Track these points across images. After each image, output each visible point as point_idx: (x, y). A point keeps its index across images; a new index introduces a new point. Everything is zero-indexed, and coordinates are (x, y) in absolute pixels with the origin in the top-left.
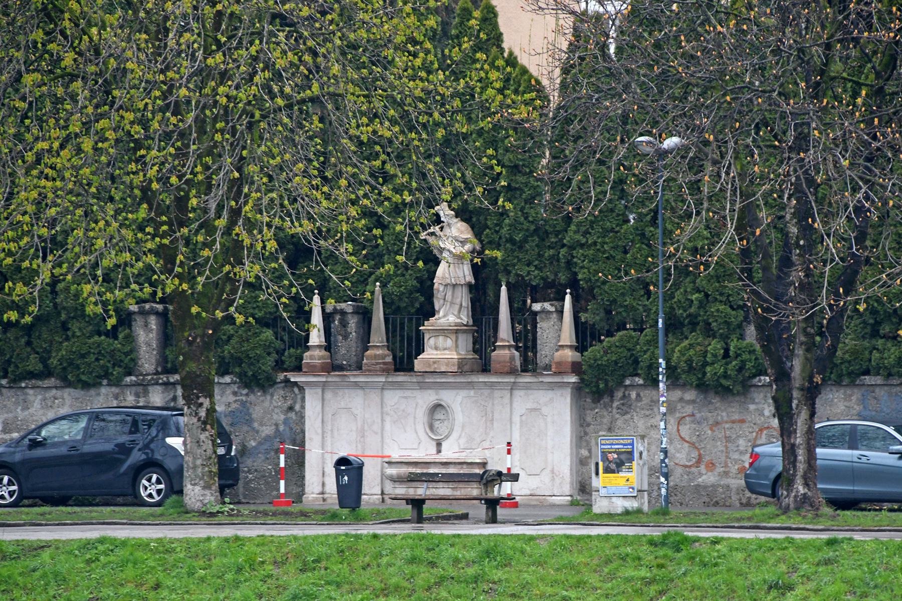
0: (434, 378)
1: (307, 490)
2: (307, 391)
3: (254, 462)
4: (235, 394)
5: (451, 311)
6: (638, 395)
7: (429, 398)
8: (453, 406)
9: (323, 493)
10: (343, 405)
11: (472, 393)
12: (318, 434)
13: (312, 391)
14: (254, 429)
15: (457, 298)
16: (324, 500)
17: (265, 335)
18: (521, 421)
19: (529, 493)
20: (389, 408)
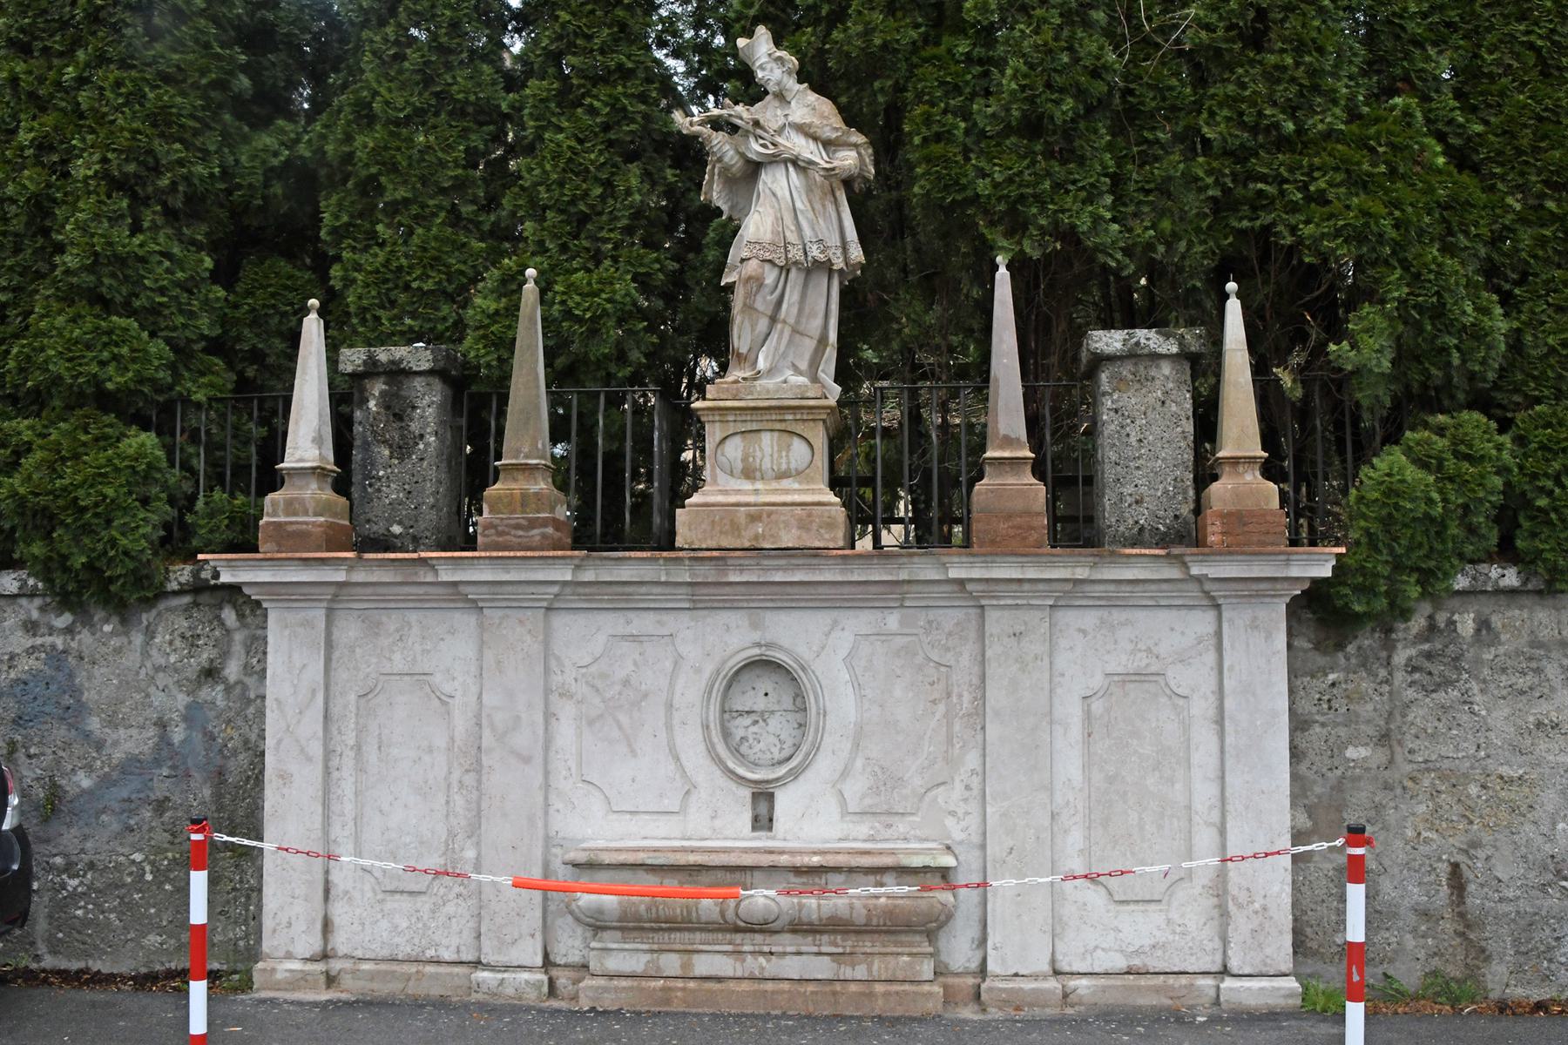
0: (752, 570)
1: (266, 946)
2: (272, 617)
3: (86, 838)
4: (31, 627)
5: (782, 356)
6: (1483, 625)
7: (729, 636)
8: (818, 667)
9: (325, 956)
10: (398, 662)
11: (893, 620)
12: (309, 759)
13: (292, 617)
14: (87, 735)
15: (813, 315)
16: (331, 980)
17: (134, 442)
18: (1088, 716)
19: (1121, 963)
20: (570, 676)
